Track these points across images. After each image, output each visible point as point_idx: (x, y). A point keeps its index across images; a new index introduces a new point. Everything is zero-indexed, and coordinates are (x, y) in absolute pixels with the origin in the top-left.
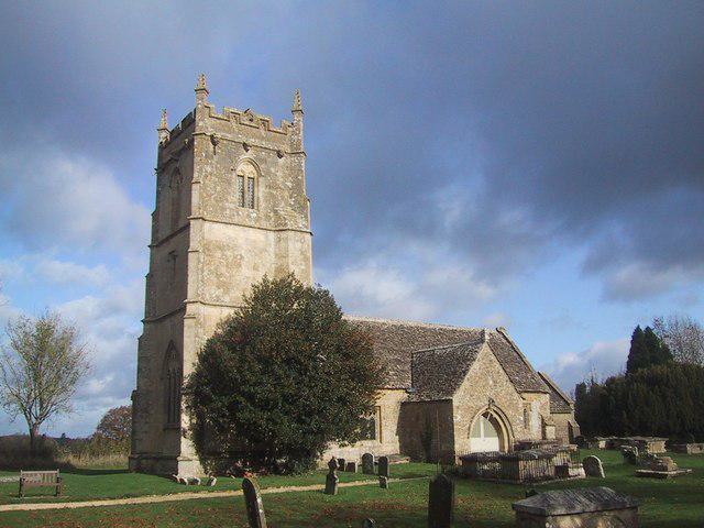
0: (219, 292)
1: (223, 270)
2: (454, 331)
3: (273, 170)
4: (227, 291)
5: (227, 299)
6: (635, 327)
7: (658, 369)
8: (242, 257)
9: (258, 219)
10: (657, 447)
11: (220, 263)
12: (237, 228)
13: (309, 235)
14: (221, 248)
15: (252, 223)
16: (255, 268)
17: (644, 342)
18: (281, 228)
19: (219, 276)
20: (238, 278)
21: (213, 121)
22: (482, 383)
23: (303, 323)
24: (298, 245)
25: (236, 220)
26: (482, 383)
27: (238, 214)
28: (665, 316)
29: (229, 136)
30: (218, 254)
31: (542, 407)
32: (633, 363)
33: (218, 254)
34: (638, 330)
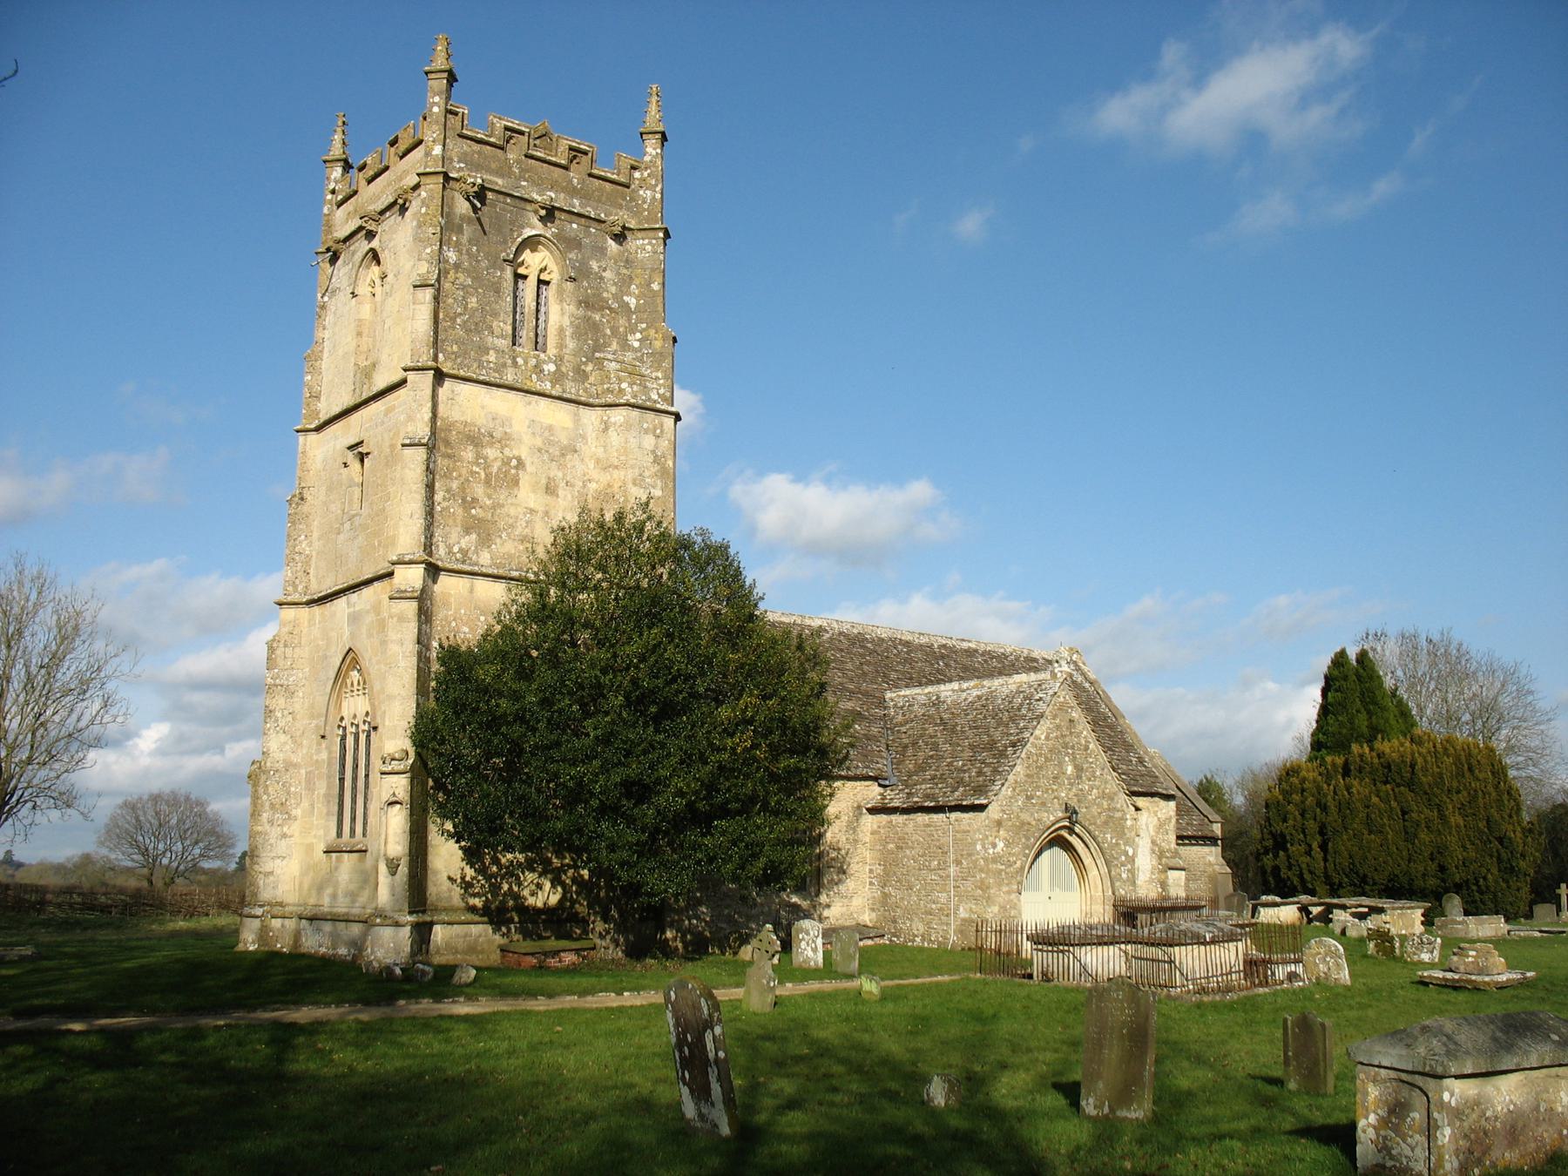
0: (469, 541)
1: (479, 491)
2: (971, 653)
3: (594, 265)
4: (485, 540)
5: (485, 559)
6: (1323, 663)
7: (1390, 747)
8: (521, 464)
9: (557, 378)
10: (1405, 920)
11: (473, 473)
12: (512, 395)
13: (670, 421)
14: (475, 439)
15: (547, 386)
16: (550, 489)
17: (1352, 691)
18: (610, 399)
19: (469, 503)
20: (512, 512)
21: (466, 146)
22: (1052, 770)
23: (654, 608)
24: (649, 441)
25: (510, 377)
26: (1052, 770)
27: (515, 364)
28: (1393, 631)
29: (500, 183)
30: (468, 454)
31: (1161, 825)
32: (1321, 741)
33: (468, 454)
34: (1340, 660)
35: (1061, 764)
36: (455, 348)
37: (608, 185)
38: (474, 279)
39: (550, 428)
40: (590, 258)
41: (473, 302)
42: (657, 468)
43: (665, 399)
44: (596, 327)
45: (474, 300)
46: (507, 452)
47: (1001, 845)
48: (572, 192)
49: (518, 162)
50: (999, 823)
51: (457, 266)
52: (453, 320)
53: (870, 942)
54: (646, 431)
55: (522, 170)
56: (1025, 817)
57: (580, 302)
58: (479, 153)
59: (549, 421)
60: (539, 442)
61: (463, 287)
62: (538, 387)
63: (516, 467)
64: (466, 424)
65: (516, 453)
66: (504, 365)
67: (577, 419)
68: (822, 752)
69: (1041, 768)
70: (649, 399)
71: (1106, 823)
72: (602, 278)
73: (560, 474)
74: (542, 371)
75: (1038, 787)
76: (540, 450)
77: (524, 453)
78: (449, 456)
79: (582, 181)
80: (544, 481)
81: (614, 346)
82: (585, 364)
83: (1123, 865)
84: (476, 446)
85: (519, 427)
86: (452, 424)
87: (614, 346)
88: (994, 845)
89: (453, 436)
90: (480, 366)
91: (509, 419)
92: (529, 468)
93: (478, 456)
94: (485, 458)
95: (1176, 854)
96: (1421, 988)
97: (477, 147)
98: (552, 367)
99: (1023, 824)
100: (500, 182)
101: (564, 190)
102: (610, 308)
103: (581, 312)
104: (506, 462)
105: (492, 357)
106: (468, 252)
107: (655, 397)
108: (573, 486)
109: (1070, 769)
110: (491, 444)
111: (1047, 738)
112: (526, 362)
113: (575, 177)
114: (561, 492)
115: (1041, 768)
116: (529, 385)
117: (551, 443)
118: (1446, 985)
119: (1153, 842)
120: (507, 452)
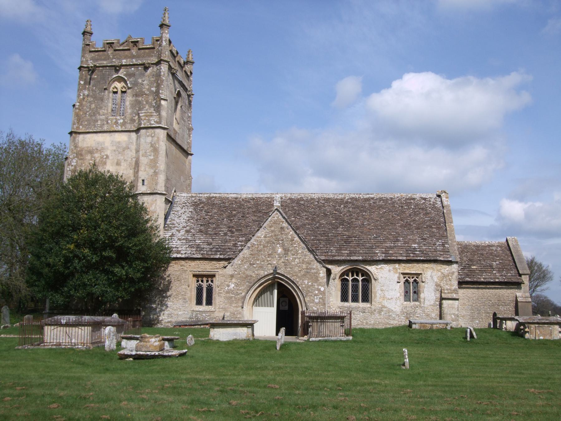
3: (140, 81)
8: (107, 157)
15: (120, 128)
21: (93, 55)
22: (268, 251)
25: (105, 128)
35: (274, 248)
36: (86, 123)
37: (147, 51)
38: (94, 98)
39: (119, 142)
40: (138, 79)
41: (93, 106)
42: (152, 148)
43: (157, 122)
44: (139, 103)
45: (94, 105)
46: (103, 154)
47: (232, 286)
48: (133, 57)
49: (112, 53)
50: (232, 276)
51: (88, 96)
52: (86, 114)
53: (199, 327)
54: (148, 136)
55: (114, 56)
56: (249, 273)
57: (133, 95)
58: (98, 55)
59: (118, 140)
60: (114, 148)
61: (90, 102)
62: (116, 129)
63: (106, 158)
64: (88, 147)
65: (106, 153)
66: (104, 124)
67: (130, 138)
68: (169, 248)
69: (260, 251)
70: (151, 124)
71: (304, 275)
72: (142, 84)
73: (122, 158)
74: (118, 123)
75: (258, 260)
76: (115, 151)
77: (108, 152)
78: (81, 159)
79: (137, 52)
80: (116, 161)
81: (147, 107)
82: (135, 117)
83: (316, 295)
84: (91, 154)
85: (107, 144)
86: (84, 148)
87: (147, 107)
88: (228, 286)
89: (84, 152)
90: (95, 127)
91: (104, 143)
92: (111, 158)
93: (92, 157)
94: (94, 157)
95: (455, 291)
96: (183, 358)
97: (97, 54)
98: (122, 121)
99: (247, 276)
100: (105, 62)
101: (129, 57)
102: (146, 94)
103: (134, 98)
104: (102, 157)
105: (99, 123)
106: (92, 90)
107: (152, 122)
108: (127, 161)
109: (280, 250)
110: (97, 152)
111: (265, 237)
112: (112, 121)
113: (134, 51)
114: (122, 164)
115: (260, 251)
116: (112, 129)
117: (119, 147)
118: (137, 357)
119: (437, 285)
120: (103, 154)
